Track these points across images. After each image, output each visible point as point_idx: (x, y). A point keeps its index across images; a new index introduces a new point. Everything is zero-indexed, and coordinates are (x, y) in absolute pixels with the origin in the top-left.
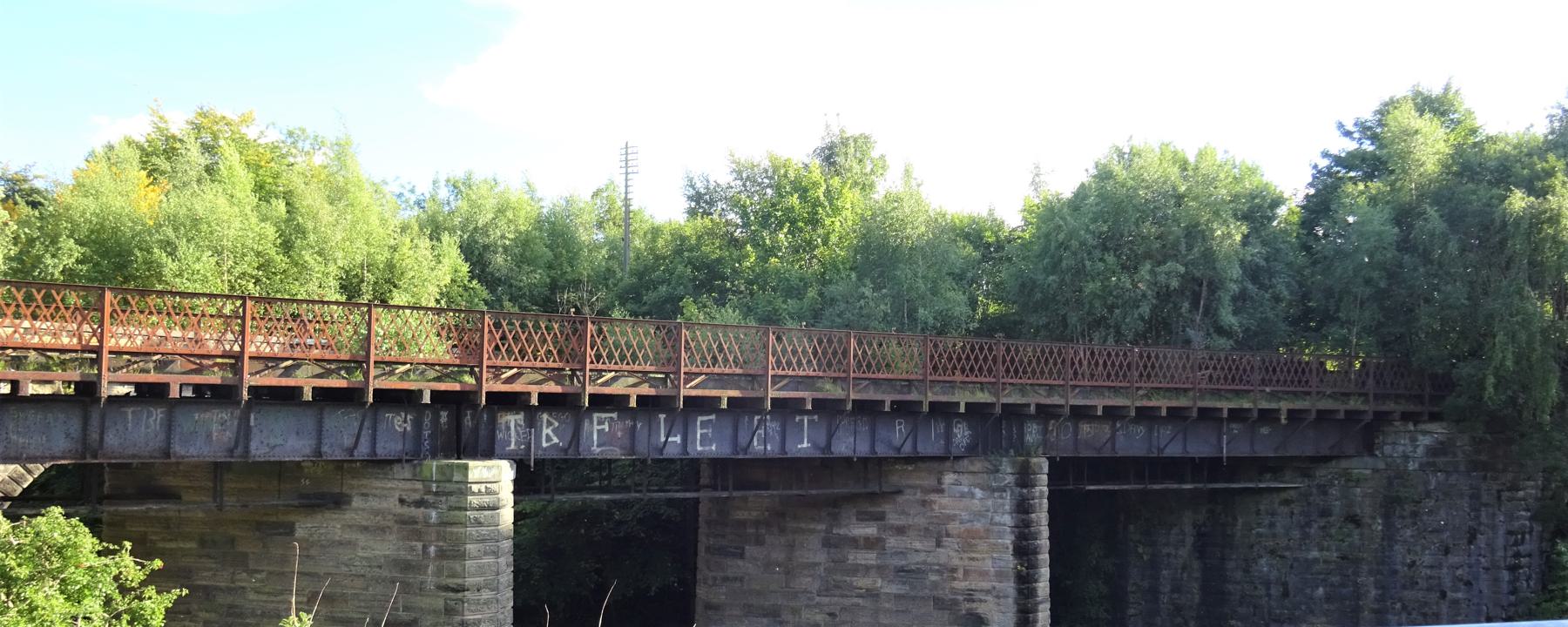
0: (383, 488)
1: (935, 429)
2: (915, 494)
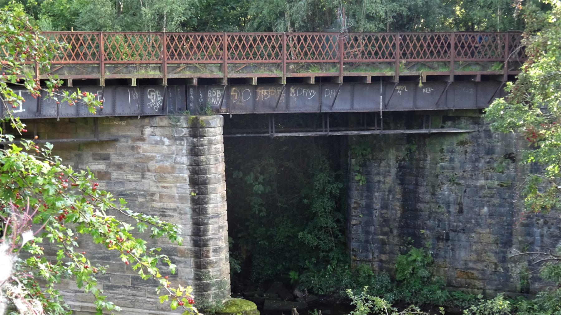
1: (132, 97)
2: (127, 142)
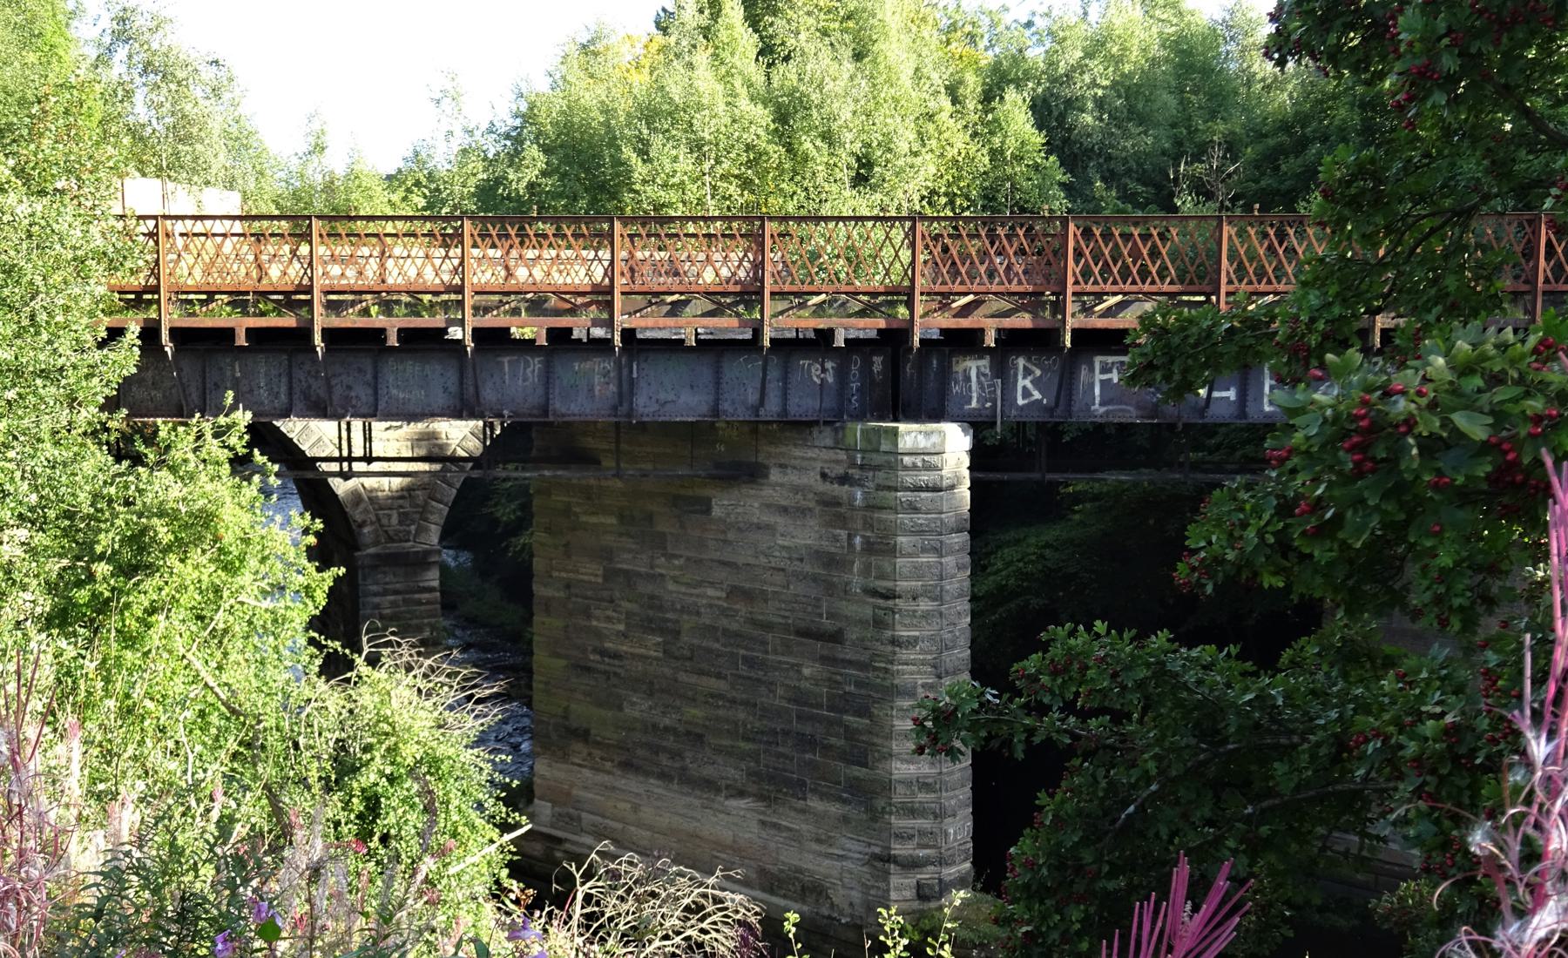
0: (803, 458)
